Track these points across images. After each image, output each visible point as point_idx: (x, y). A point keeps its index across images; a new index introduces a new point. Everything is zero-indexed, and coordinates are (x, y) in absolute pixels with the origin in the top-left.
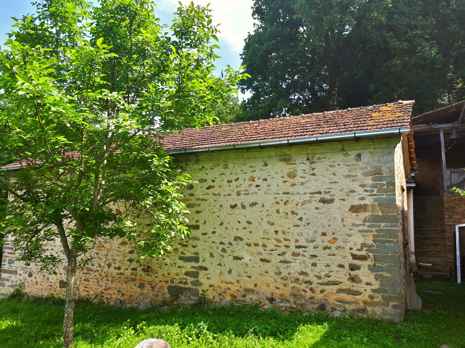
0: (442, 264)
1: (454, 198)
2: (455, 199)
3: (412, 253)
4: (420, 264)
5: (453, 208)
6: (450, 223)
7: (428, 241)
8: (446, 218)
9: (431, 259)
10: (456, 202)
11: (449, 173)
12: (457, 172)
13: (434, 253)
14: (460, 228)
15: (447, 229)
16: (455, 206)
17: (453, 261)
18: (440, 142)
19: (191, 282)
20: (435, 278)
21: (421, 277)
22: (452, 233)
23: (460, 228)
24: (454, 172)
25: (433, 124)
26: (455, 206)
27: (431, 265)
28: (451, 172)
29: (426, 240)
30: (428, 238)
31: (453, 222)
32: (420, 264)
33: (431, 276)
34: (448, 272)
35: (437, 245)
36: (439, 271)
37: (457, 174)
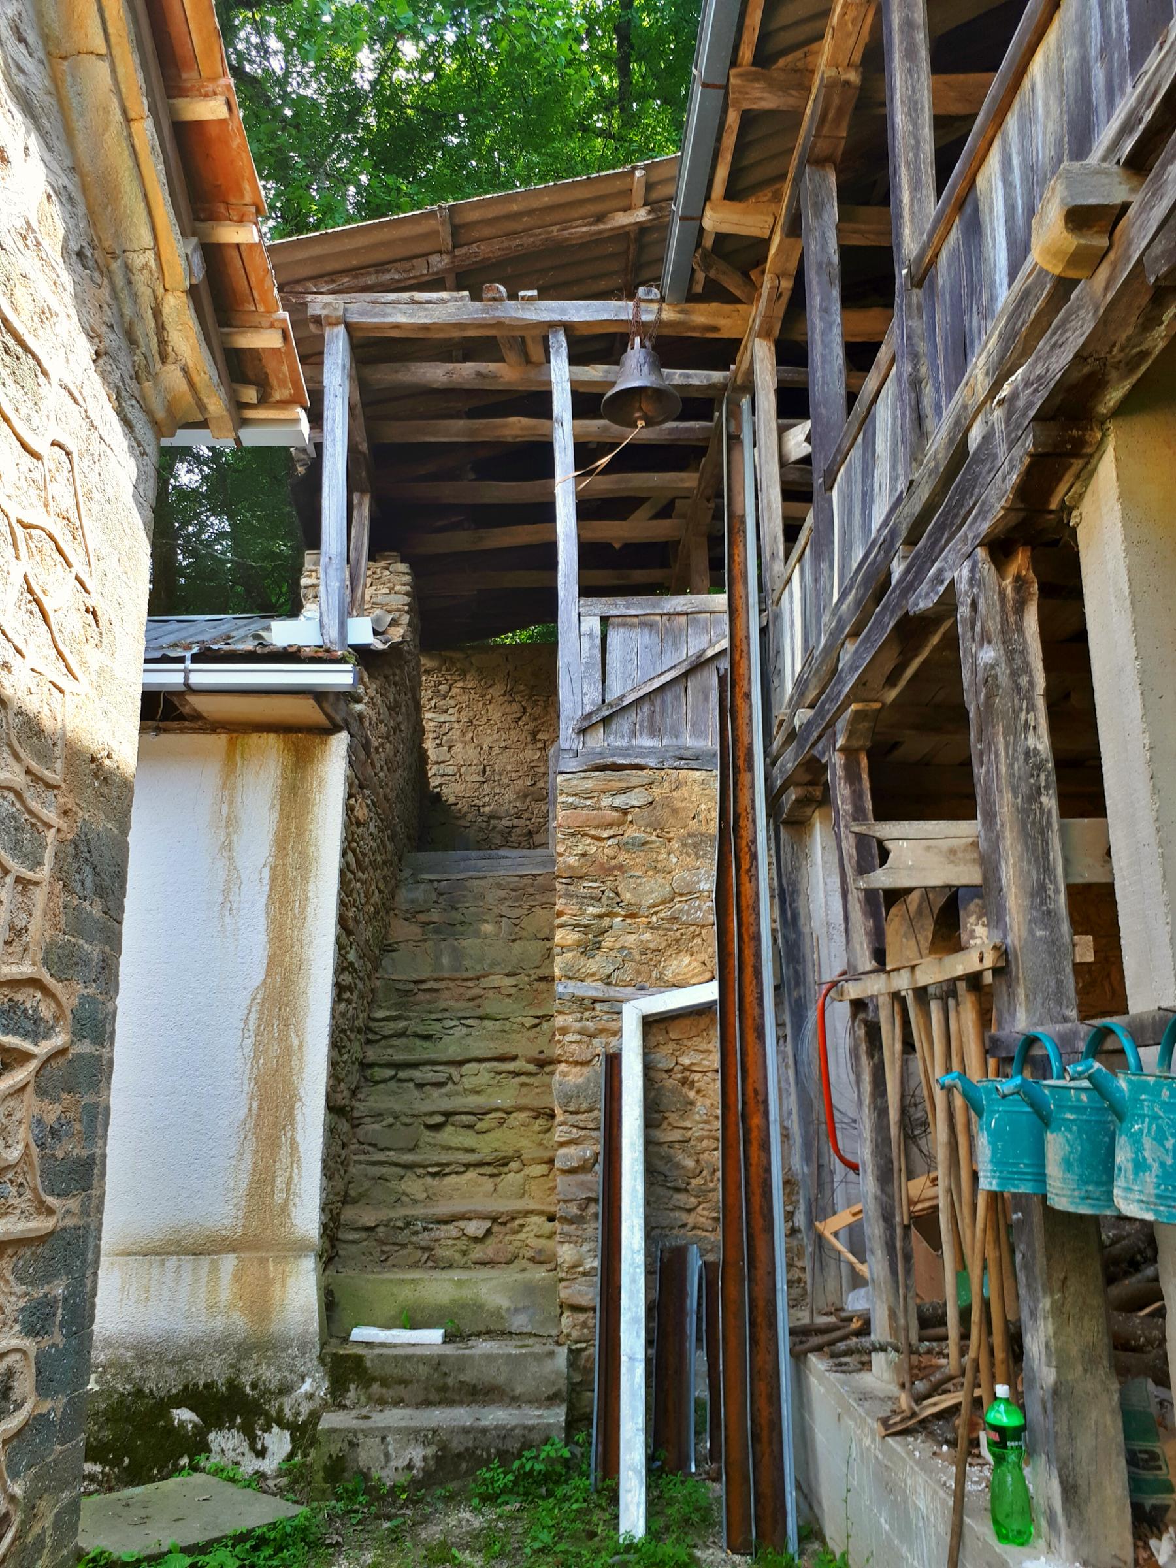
0: (519, 1322)
1: (620, 801)
2: (625, 812)
3: (299, 1248)
4: (360, 1333)
5: (610, 870)
6: (589, 989)
7: (448, 1135)
8: (564, 949)
9: (438, 1288)
10: (631, 832)
11: (592, 624)
12: (644, 623)
13: (475, 1228)
14: (651, 1024)
15: (564, 1031)
16: (624, 857)
17: (587, 1292)
18: (551, 548)
19: (989, 1192)
20: (453, 1468)
21: (336, 1469)
22: (599, 1065)
23: (651, 1024)
24: (624, 621)
25: (513, 296)
26: (624, 857)
27: (434, 1336)
28: (605, 620)
29: (437, 1127)
30: (447, 1114)
31: (607, 981)
32: (360, 1333)
33: (417, 1454)
34: (553, 1399)
35: (500, 1164)
36: (481, 1394)
37: (644, 638)
